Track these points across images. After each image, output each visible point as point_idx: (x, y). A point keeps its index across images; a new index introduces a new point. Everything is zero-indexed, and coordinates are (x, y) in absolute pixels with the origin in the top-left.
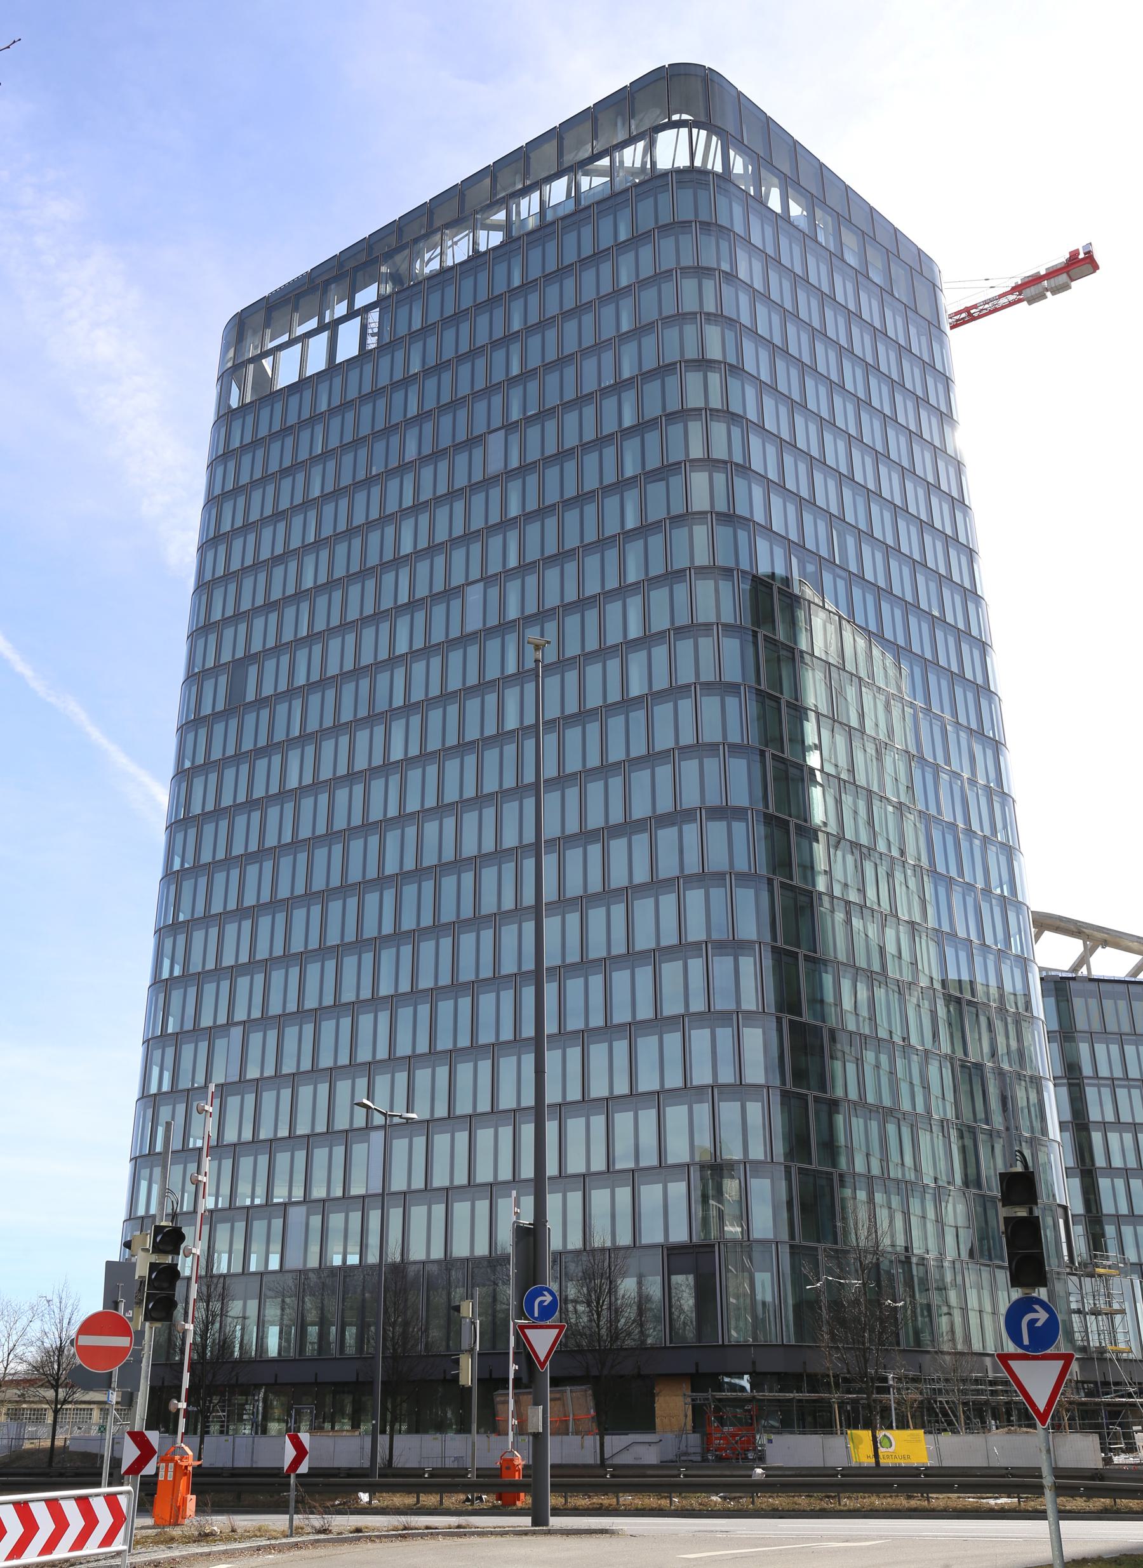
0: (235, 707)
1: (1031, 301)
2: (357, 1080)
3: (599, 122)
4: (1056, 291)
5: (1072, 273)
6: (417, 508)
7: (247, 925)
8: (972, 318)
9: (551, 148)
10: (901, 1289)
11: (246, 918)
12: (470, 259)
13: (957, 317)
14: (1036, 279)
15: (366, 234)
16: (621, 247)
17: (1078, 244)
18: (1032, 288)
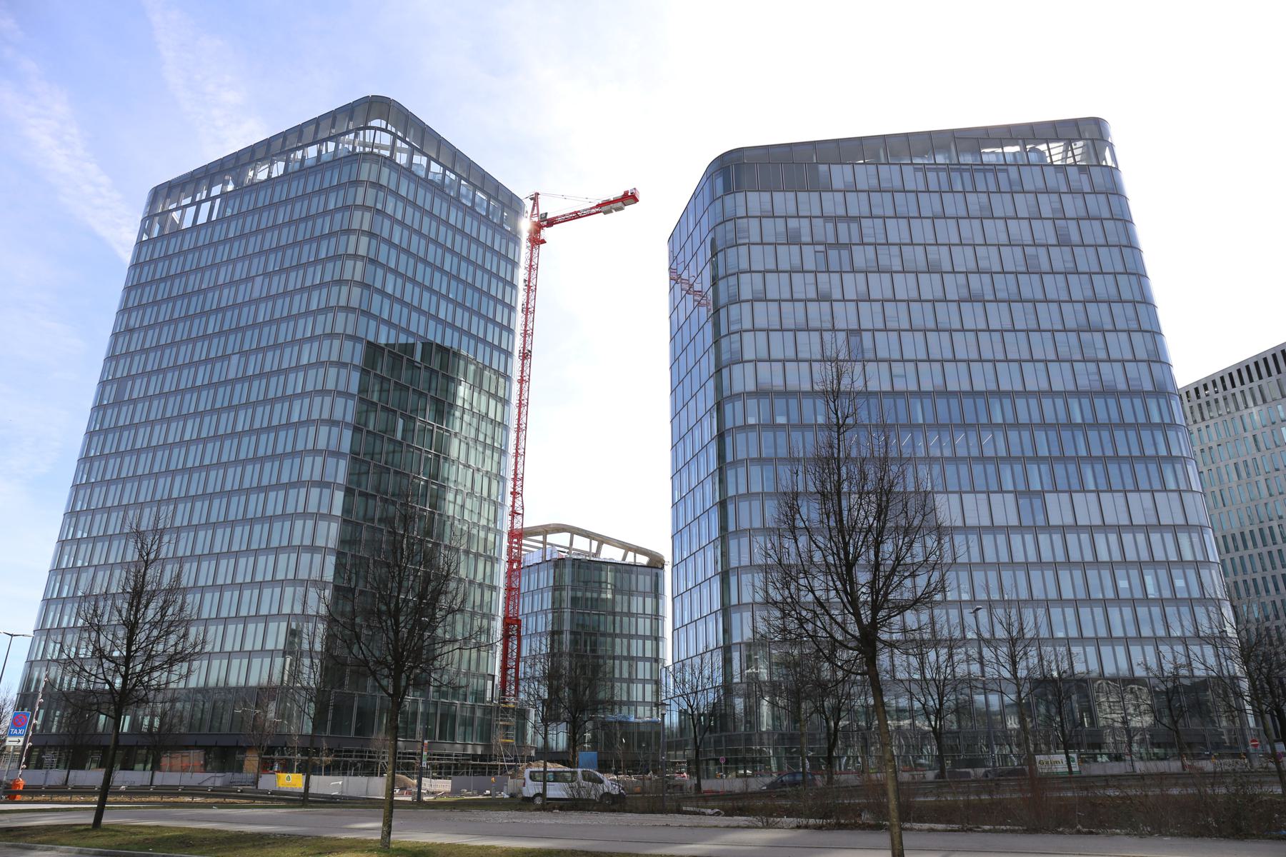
0: (118, 403)
4: (617, 210)
6: (322, 285)
7: (262, 496)
9: (313, 128)
12: (266, 181)
14: (608, 203)
17: (629, 188)
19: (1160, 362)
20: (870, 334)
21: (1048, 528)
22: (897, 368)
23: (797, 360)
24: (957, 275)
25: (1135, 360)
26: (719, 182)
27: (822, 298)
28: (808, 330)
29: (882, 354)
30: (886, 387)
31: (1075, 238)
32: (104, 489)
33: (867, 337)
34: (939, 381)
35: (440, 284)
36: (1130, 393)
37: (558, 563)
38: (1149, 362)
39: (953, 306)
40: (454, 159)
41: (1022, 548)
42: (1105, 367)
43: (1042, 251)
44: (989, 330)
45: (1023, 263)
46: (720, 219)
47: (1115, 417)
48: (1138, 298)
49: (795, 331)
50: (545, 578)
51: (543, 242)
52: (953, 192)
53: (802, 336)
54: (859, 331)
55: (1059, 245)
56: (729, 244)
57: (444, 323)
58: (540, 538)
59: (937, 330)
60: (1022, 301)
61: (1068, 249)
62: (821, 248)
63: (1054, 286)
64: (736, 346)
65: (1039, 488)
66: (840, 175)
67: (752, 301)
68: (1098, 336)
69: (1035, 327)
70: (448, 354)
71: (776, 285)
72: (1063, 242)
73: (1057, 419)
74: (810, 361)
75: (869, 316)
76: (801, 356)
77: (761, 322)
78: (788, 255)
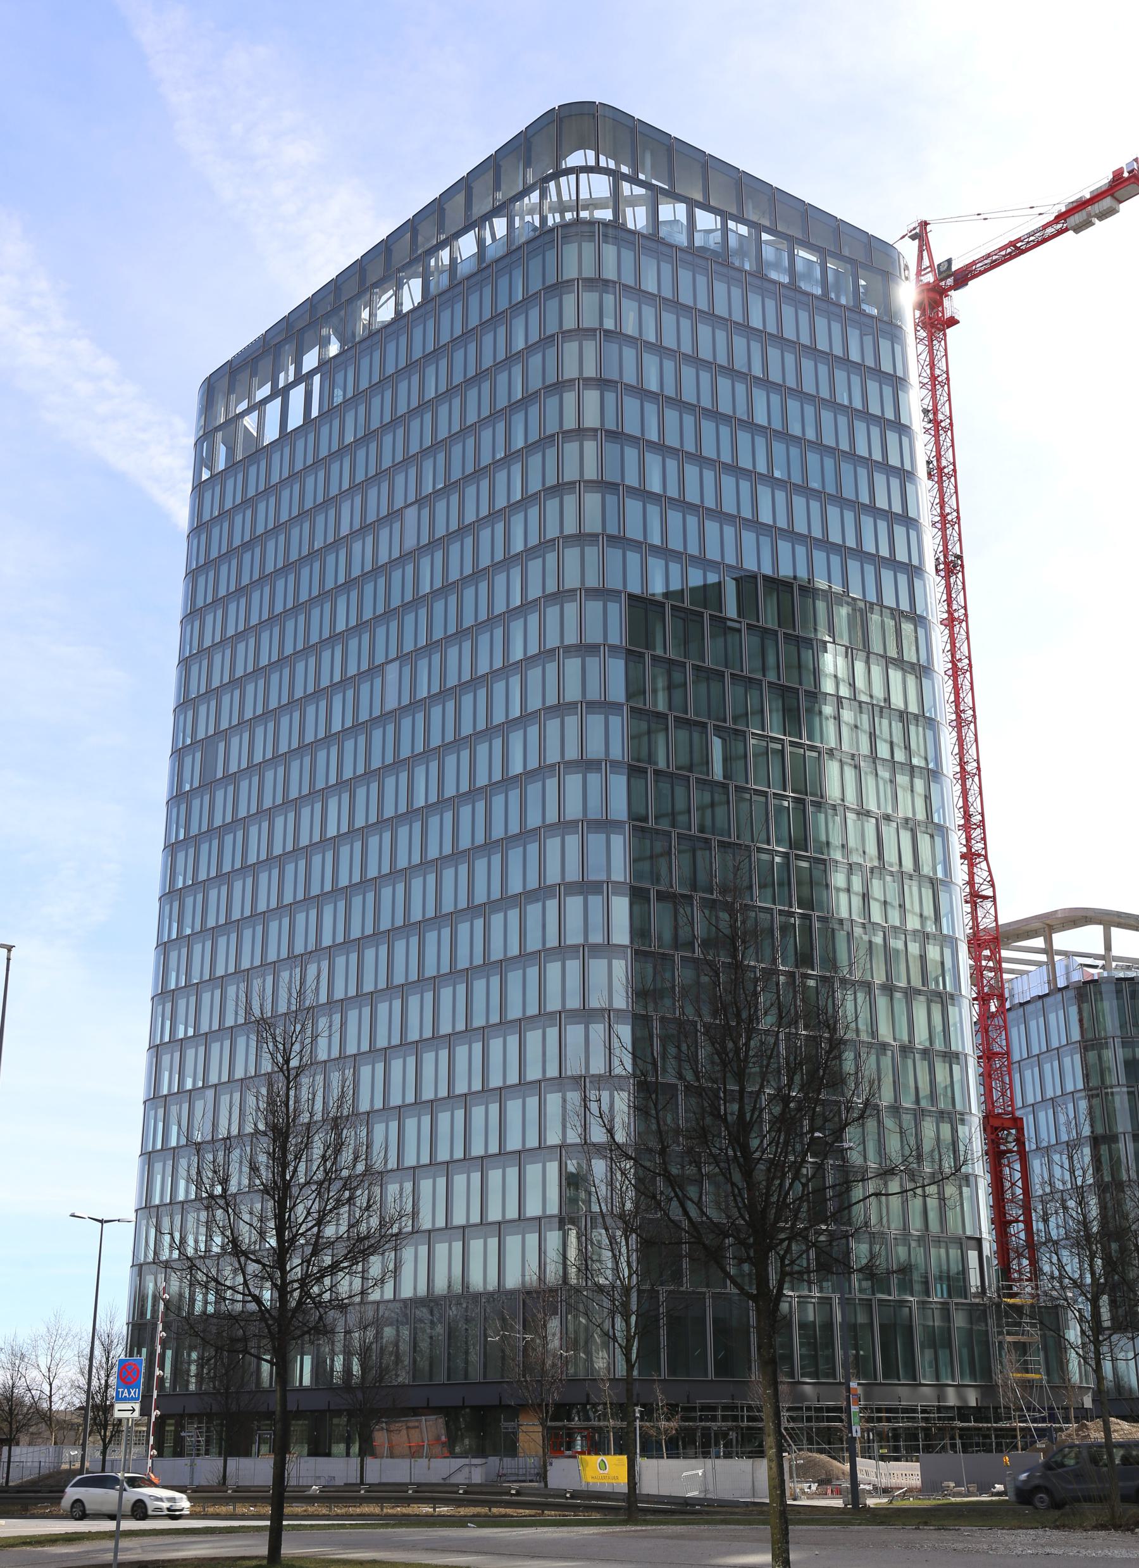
0: (208, 785)
1: (1077, 229)
2: (528, 1099)
3: (503, 170)
4: (1102, 216)
5: (1117, 195)
8: (1022, 252)
10: (917, 1287)
11: (478, 917)
12: (394, 321)
13: (1003, 253)
14: (1080, 206)
15: (333, 275)
16: (515, 308)
18: (1076, 216)
51: (952, 322)
57: (772, 531)
58: (1039, 942)
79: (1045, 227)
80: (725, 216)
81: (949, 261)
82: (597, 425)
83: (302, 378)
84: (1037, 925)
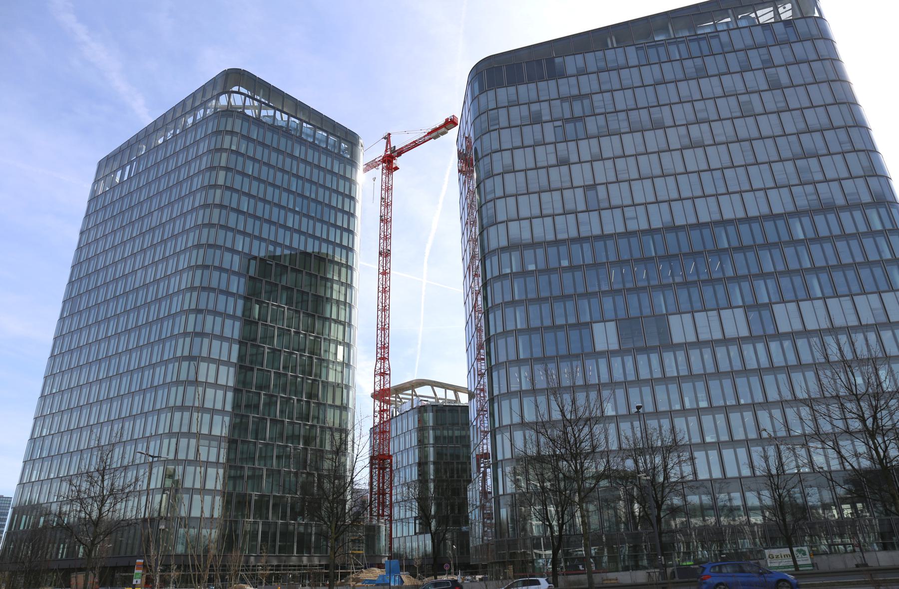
0: (71, 315)
1: (435, 138)
14: (436, 130)
17: (448, 116)
19: (877, 175)
20: (604, 187)
21: (779, 336)
22: (629, 212)
23: (542, 216)
24: (679, 128)
25: (851, 177)
26: (476, 85)
27: (563, 162)
28: (551, 190)
29: (616, 201)
30: (621, 229)
31: (784, 80)
32: (166, 390)
33: (601, 190)
34: (667, 218)
35: (286, 199)
36: (849, 207)
37: (422, 410)
38: (865, 177)
39: (677, 154)
40: (298, 108)
41: (756, 355)
42: (822, 188)
43: (755, 98)
44: (710, 170)
45: (738, 109)
46: (478, 114)
47: (836, 231)
48: (851, 123)
49: (539, 193)
50: (412, 422)
51: (396, 168)
52: (671, 61)
53: (545, 196)
54: (594, 186)
55: (770, 90)
56: (484, 132)
57: (292, 230)
58: (410, 392)
59: (664, 176)
60: (738, 141)
61: (779, 92)
62: (559, 123)
63: (768, 125)
64: (491, 211)
65: (766, 300)
66: (572, 63)
67: (502, 174)
68: (813, 162)
69: (753, 161)
70: (323, 260)
71: (522, 159)
72: (774, 86)
73: (779, 238)
74: (553, 216)
75: (602, 172)
76: (545, 212)
77: (510, 189)
78: (531, 134)
79: (424, 137)
80: (289, 115)
81: (395, 147)
82: (223, 184)
83: (130, 163)
84: (408, 385)
